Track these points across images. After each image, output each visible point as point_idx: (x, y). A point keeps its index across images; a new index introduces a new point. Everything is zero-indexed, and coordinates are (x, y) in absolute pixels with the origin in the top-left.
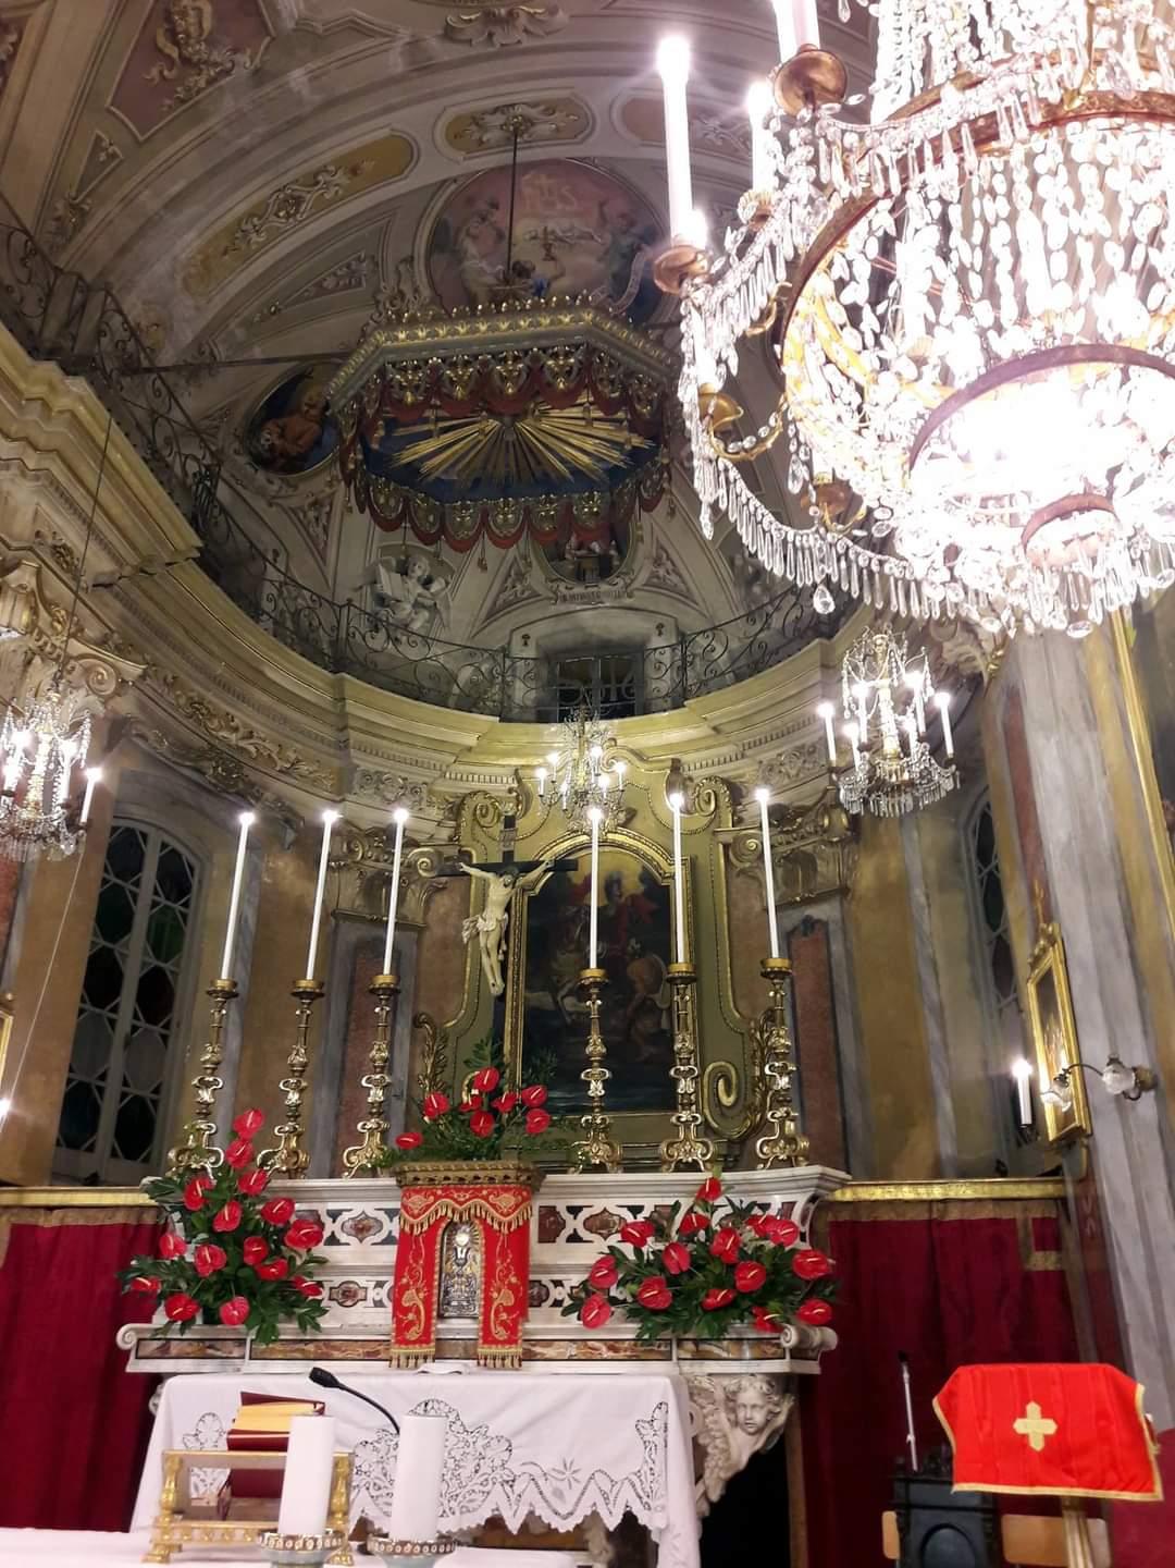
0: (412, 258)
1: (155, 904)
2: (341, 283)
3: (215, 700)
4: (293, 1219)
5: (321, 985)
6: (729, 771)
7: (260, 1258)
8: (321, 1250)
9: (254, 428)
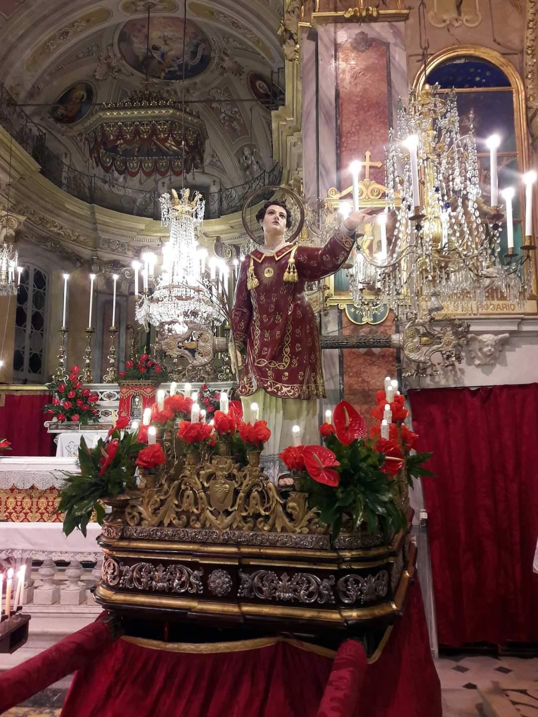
0: (113, 44)
1: (34, 290)
2: (86, 55)
3: (48, 217)
4: (90, 394)
5: (93, 329)
6: (236, 242)
7: (82, 405)
8: (98, 402)
9: (55, 109)
